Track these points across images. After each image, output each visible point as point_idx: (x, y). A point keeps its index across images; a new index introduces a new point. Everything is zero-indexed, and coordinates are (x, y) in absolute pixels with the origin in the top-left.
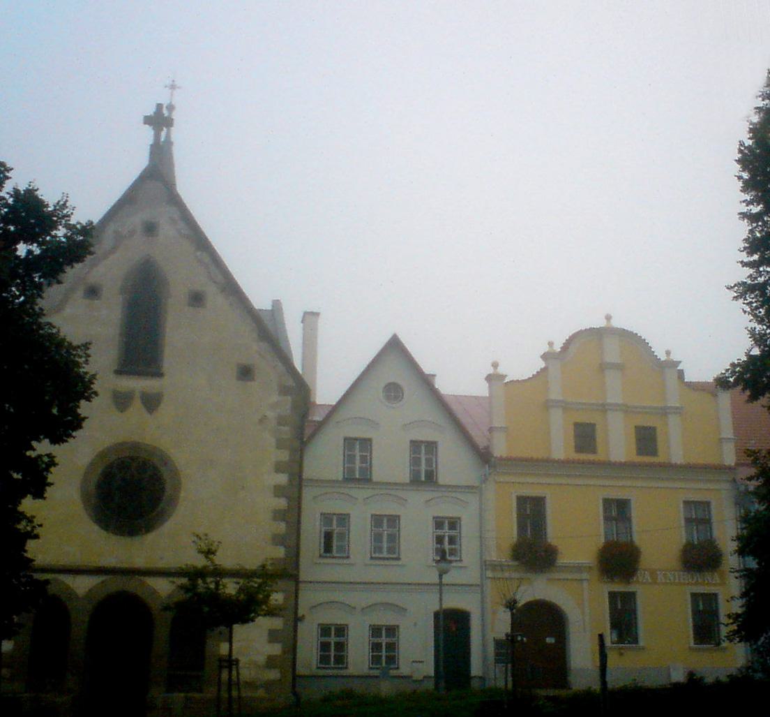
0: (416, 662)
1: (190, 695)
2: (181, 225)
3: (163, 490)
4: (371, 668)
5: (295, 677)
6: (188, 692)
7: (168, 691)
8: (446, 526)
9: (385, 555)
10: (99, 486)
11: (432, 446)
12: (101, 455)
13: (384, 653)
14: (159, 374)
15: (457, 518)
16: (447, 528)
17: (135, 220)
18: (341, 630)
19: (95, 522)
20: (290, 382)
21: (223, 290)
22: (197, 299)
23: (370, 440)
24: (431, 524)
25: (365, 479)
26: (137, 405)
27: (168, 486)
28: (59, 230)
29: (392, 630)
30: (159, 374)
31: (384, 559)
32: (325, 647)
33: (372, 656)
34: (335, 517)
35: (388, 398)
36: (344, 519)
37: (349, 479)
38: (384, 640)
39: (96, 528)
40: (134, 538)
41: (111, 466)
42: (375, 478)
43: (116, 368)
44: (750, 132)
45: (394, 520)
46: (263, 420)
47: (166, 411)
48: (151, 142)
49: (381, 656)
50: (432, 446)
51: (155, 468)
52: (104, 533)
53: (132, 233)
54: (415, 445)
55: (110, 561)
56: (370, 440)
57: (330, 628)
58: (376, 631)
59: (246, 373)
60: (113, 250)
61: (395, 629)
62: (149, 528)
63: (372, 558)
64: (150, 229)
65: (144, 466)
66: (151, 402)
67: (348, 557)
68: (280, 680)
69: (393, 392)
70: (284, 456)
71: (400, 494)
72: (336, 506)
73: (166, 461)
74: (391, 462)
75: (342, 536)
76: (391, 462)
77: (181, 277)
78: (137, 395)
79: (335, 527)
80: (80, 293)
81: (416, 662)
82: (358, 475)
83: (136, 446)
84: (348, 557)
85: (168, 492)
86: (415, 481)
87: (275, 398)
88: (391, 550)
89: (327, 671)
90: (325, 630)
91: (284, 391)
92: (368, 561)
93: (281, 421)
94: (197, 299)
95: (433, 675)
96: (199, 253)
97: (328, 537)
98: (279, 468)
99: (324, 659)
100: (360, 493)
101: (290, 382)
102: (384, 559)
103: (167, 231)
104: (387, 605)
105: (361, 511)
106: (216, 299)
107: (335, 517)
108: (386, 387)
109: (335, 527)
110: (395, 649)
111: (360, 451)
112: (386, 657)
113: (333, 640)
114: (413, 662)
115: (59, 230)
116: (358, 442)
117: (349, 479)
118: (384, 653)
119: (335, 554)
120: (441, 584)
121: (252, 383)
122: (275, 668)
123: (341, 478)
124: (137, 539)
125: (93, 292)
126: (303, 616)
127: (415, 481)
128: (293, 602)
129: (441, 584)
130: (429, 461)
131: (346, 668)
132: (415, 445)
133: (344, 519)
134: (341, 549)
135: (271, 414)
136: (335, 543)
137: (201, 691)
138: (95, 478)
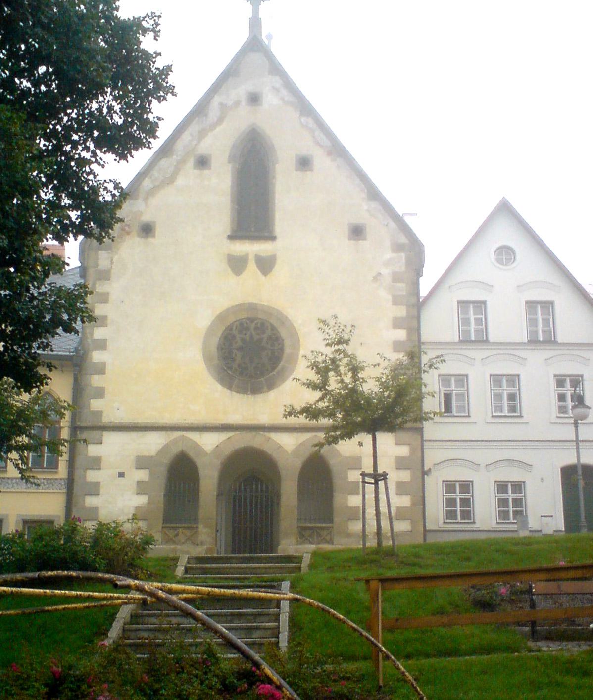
0: (544, 516)
1: (320, 546)
2: (284, 92)
3: (282, 350)
4: (498, 523)
5: (425, 530)
6: (319, 543)
7: (298, 543)
8: (568, 383)
9: (506, 413)
10: (220, 348)
11: (548, 306)
12: (220, 318)
13: (511, 509)
14: (273, 238)
15: (578, 376)
16: (569, 386)
17: (239, 91)
18: (466, 486)
19: (218, 381)
20: (403, 240)
21: (329, 154)
22: (304, 163)
23: (484, 303)
24: (553, 384)
25: (483, 340)
26: (252, 266)
27: (287, 343)
28: (76, 239)
29: (518, 486)
30: (273, 238)
31: (505, 417)
32: (451, 502)
33: (499, 511)
34: (453, 379)
35: (499, 261)
36: (462, 379)
37: (465, 341)
38: (510, 496)
39: (219, 387)
40: (256, 395)
41: (230, 328)
42: (491, 338)
43: (229, 234)
44: (97, 485)
45: (513, 379)
46: (377, 277)
47: (280, 272)
48: (251, 16)
49: (508, 511)
50: (548, 306)
51: (273, 328)
52: (227, 392)
53: (237, 104)
54: (531, 305)
55: (235, 418)
56: (484, 303)
57: (455, 485)
58: (502, 487)
59: (357, 232)
60: (220, 120)
61: (520, 486)
62: (271, 386)
63: (493, 417)
64: (254, 99)
65: (262, 326)
66: (266, 265)
67: (469, 416)
68: (411, 531)
69: (505, 254)
70: (402, 312)
71: (522, 354)
72: (451, 367)
73: (284, 320)
74: (507, 321)
75: (460, 396)
76: (507, 321)
77: (287, 141)
78: (252, 258)
79: (453, 387)
80: (191, 162)
81: (544, 516)
82: (476, 337)
83: (252, 307)
84: (469, 416)
85: (288, 350)
86: (533, 341)
87: (389, 255)
88: (513, 409)
89: (227, 584)
90: (450, 486)
91: (398, 248)
92: (489, 420)
93: (396, 278)
94: (304, 163)
95: (563, 529)
96: (303, 119)
97: (448, 397)
98: (397, 323)
99: (451, 515)
100: (477, 354)
101: (403, 240)
102: (505, 417)
103: (270, 100)
104: (511, 461)
105: (478, 372)
106: (322, 162)
107: (453, 379)
108: (497, 249)
109: (453, 387)
110: (521, 503)
111: (474, 314)
112: (513, 511)
113: (458, 496)
114: (542, 516)
115: (76, 239)
116: (471, 306)
117: (465, 341)
118: (511, 509)
119: (454, 412)
120: (577, 441)
121: (364, 242)
122: (405, 519)
123: (457, 339)
124: (260, 397)
125: (203, 162)
126: (430, 469)
127: (533, 341)
128: (420, 455)
129: (577, 441)
130: (546, 322)
131: (474, 523)
132: (531, 305)
133: (462, 379)
134: (461, 408)
135: (386, 271)
136: (454, 404)
137: (331, 542)
138: (215, 340)
